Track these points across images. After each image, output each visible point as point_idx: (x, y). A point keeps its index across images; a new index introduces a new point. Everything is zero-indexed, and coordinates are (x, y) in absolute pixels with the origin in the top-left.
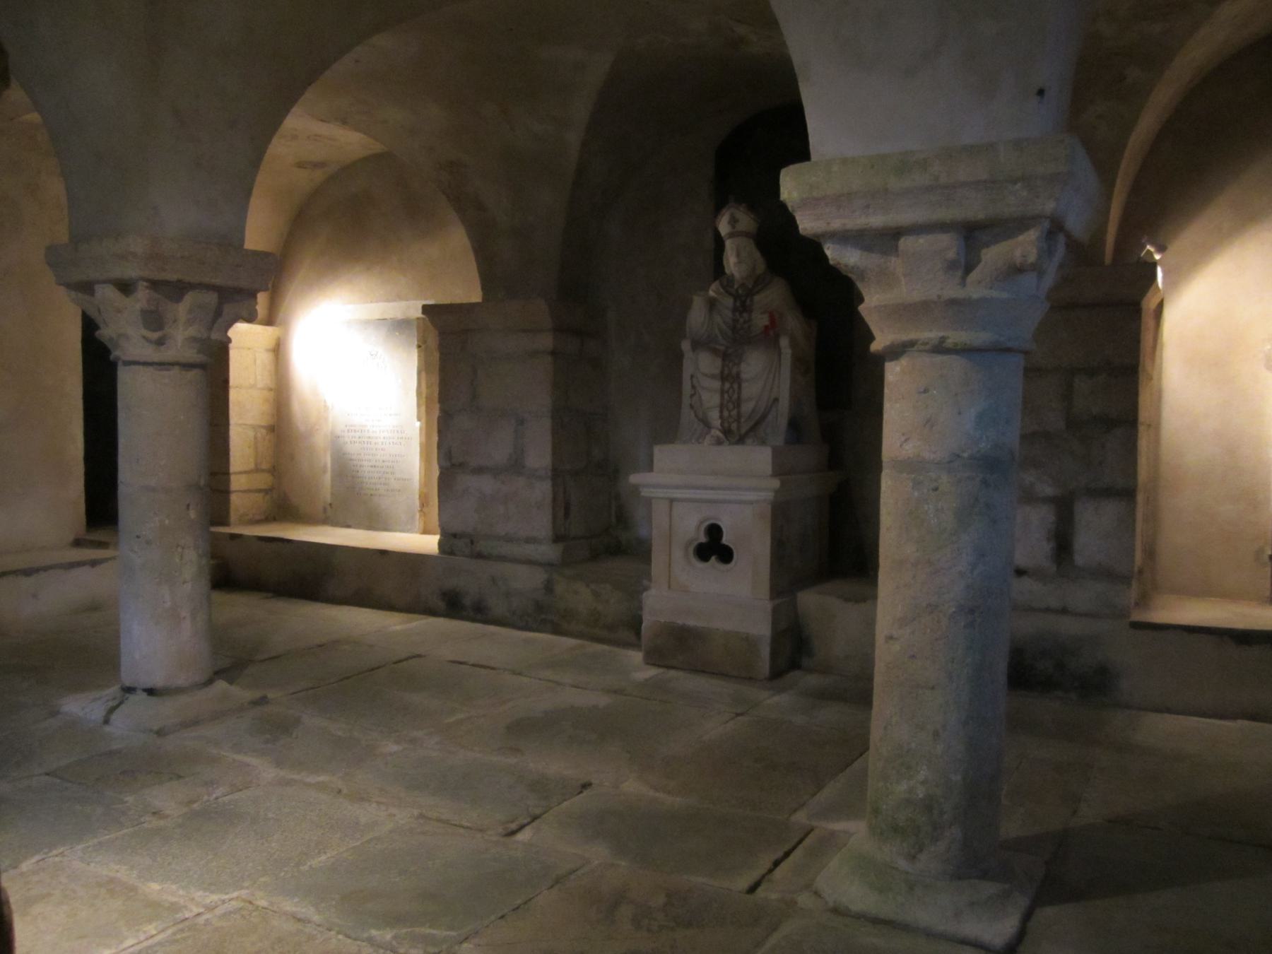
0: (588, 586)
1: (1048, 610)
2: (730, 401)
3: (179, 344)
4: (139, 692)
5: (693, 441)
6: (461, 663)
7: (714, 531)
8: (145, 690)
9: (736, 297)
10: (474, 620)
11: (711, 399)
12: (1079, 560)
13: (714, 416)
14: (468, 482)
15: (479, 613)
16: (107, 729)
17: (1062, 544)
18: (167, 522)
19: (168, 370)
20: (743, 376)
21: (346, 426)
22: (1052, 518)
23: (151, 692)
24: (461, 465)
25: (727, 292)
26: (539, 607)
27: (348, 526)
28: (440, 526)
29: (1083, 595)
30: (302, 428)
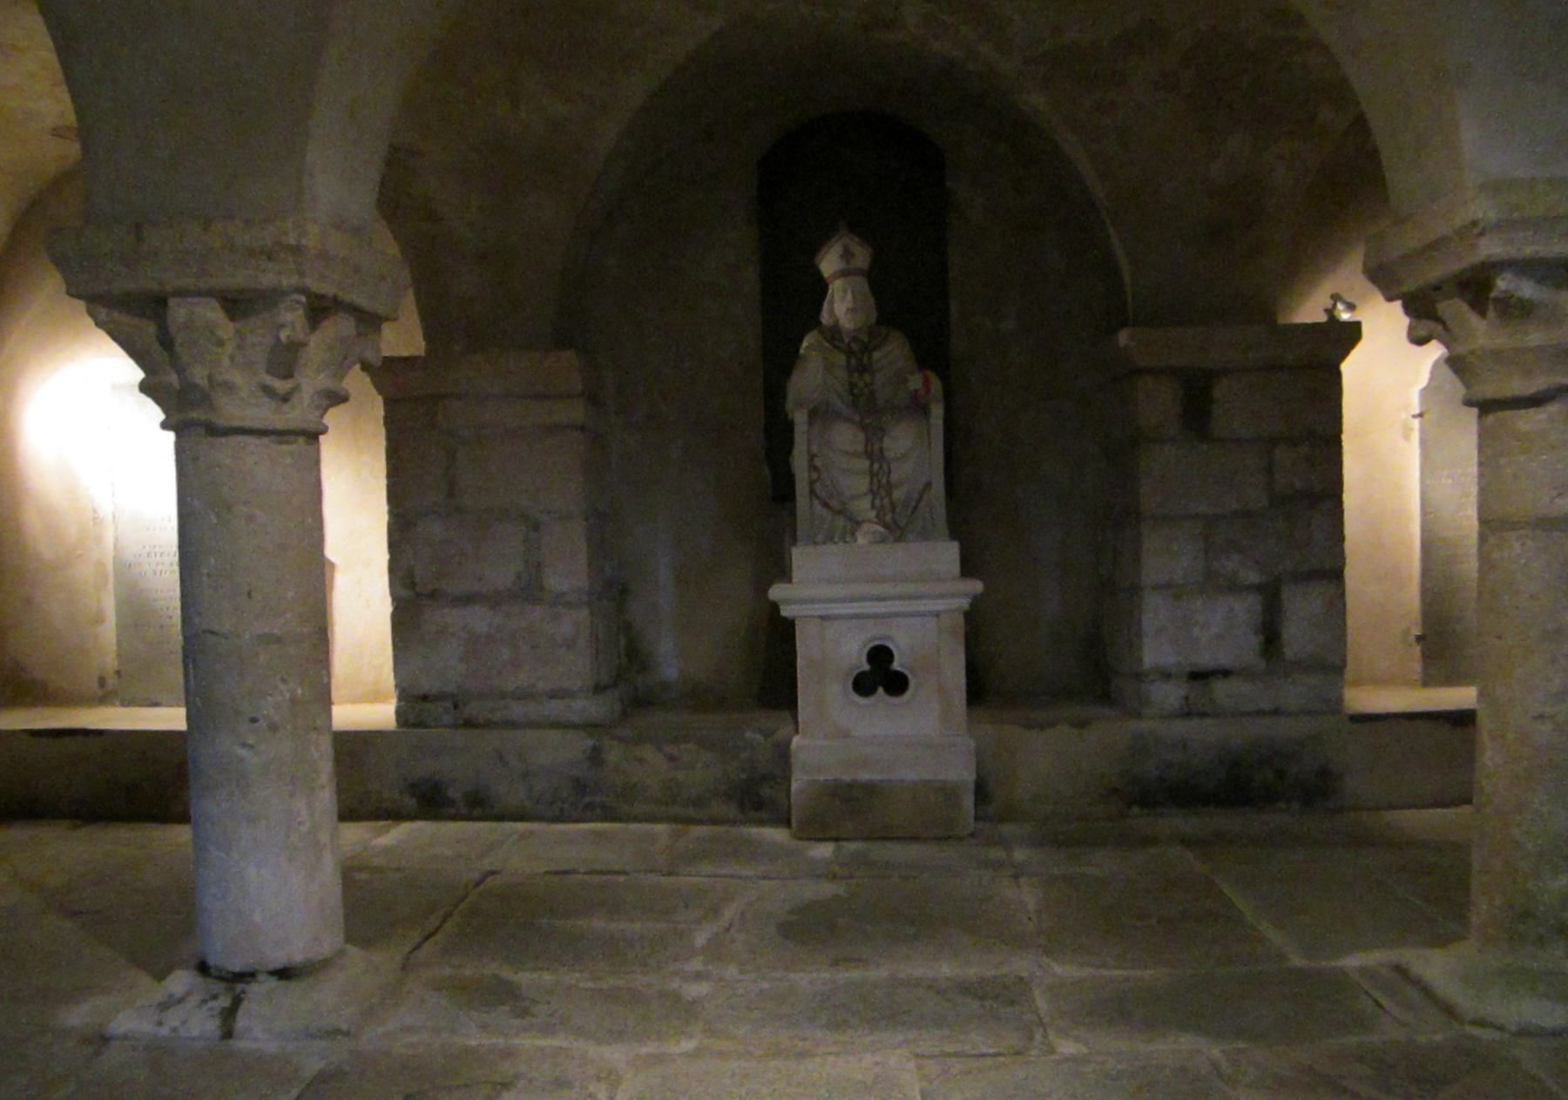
0: (660, 749)
1: (1260, 713)
2: (880, 487)
3: (306, 404)
4: (260, 978)
5: (836, 540)
6: (565, 872)
7: (880, 655)
9: (850, 353)
10: (469, 818)
11: (854, 482)
12: (1289, 652)
13: (863, 507)
15: (479, 806)
16: (241, 1044)
17: (1271, 638)
18: (299, 691)
19: (288, 443)
20: (889, 454)
21: (144, 547)
23: (284, 974)
24: (433, 595)
25: (835, 346)
26: (580, 786)
27: (156, 704)
28: (397, 686)
29: (1293, 692)
30: (48, 552)
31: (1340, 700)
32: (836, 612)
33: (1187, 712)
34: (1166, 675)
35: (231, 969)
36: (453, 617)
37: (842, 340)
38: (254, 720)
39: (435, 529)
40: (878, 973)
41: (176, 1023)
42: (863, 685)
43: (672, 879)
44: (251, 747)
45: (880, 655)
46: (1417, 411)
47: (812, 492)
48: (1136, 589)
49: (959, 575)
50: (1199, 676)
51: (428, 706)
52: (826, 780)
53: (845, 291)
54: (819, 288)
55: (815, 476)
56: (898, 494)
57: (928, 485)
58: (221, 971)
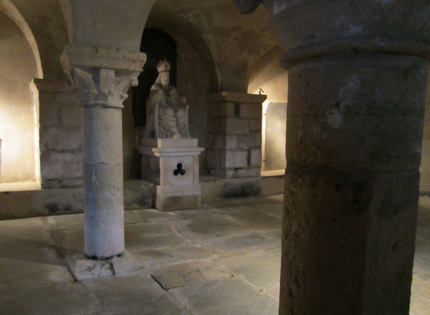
1: (246, 177)
4: (114, 257)
8: (117, 256)
9: (165, 91)
11: (172, 124)
13: (174, 130)
14: (55, 156)
17: (249, 160)
22: (247, 154)
29: (252, 172)
31: (260, 173)
32: (172, 155)
33: (234, 177)
34: (230, 169)
35: (106, 256)
36: (60, 156)
37: (163, 88)
38: (114, 187)
39: (53, 131)
40: (229, 237)
41: (98, 274)
42: (176, 173)
43: (147, 223)
44: (114, 195)
45: (179, 166)
46: (265, 114)
47: (160, 125)
48: (225, 150)
49: (197, 145)
50: (236, 169)
51: (51, 182)
52: (169, 196)
53: (165, 75)
54: (156, 74)
55: (161, 121)
56: (181, 126)
57: (185, 124)
58: (102, 257)
